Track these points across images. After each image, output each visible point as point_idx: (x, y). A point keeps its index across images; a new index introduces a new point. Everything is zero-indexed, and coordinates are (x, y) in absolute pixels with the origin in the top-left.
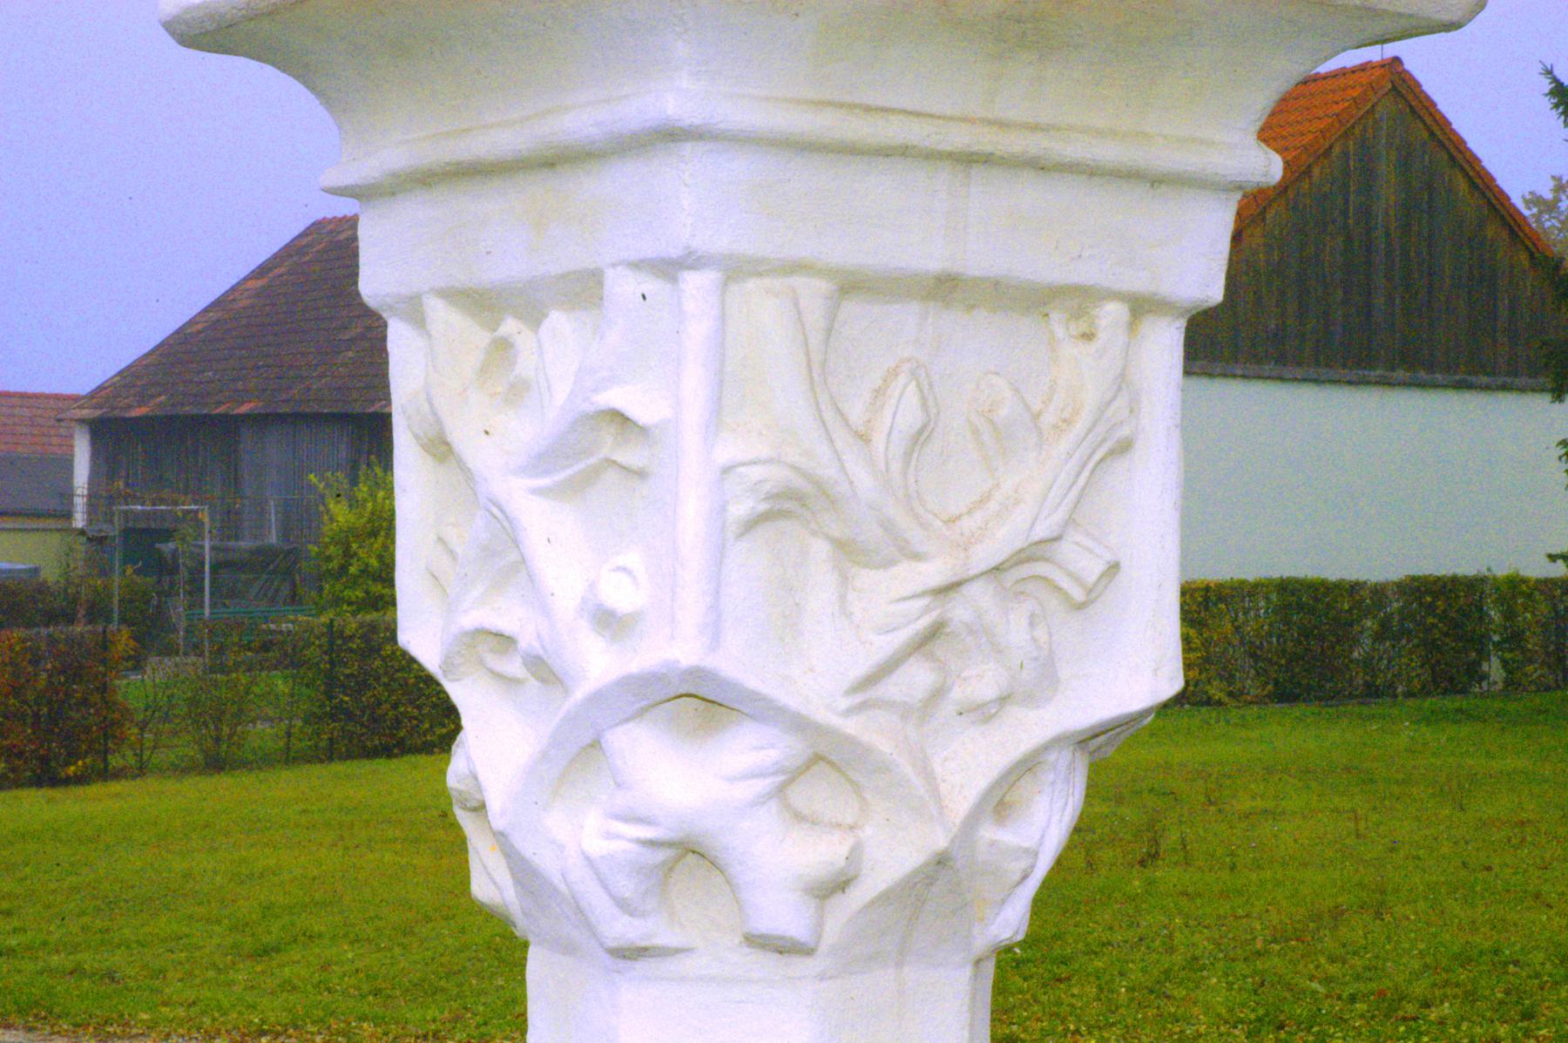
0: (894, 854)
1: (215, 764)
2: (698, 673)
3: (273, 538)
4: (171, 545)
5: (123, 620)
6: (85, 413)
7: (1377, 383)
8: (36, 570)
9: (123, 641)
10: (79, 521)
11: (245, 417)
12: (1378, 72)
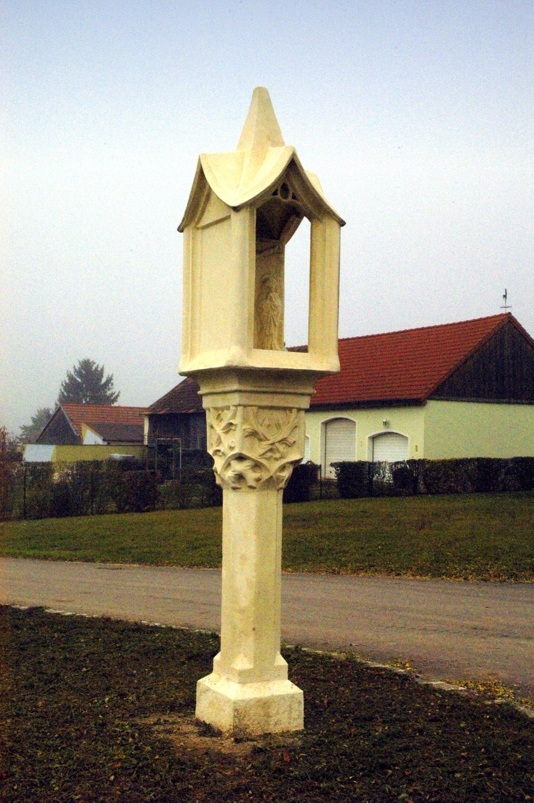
0: (265, 476)
1: (183, 507)
2: (240, 454)
3: (198, 448)
4: (171, 449)
5: (158, 469)
6: (147, 413)
7: (506, 403)
8: (134, 457)
9: (159, 473)
10: (146, 443)
11: (192, 414)
12: (505, 316)
